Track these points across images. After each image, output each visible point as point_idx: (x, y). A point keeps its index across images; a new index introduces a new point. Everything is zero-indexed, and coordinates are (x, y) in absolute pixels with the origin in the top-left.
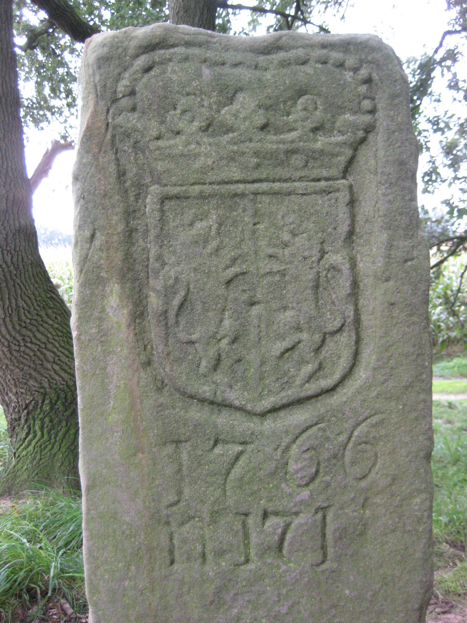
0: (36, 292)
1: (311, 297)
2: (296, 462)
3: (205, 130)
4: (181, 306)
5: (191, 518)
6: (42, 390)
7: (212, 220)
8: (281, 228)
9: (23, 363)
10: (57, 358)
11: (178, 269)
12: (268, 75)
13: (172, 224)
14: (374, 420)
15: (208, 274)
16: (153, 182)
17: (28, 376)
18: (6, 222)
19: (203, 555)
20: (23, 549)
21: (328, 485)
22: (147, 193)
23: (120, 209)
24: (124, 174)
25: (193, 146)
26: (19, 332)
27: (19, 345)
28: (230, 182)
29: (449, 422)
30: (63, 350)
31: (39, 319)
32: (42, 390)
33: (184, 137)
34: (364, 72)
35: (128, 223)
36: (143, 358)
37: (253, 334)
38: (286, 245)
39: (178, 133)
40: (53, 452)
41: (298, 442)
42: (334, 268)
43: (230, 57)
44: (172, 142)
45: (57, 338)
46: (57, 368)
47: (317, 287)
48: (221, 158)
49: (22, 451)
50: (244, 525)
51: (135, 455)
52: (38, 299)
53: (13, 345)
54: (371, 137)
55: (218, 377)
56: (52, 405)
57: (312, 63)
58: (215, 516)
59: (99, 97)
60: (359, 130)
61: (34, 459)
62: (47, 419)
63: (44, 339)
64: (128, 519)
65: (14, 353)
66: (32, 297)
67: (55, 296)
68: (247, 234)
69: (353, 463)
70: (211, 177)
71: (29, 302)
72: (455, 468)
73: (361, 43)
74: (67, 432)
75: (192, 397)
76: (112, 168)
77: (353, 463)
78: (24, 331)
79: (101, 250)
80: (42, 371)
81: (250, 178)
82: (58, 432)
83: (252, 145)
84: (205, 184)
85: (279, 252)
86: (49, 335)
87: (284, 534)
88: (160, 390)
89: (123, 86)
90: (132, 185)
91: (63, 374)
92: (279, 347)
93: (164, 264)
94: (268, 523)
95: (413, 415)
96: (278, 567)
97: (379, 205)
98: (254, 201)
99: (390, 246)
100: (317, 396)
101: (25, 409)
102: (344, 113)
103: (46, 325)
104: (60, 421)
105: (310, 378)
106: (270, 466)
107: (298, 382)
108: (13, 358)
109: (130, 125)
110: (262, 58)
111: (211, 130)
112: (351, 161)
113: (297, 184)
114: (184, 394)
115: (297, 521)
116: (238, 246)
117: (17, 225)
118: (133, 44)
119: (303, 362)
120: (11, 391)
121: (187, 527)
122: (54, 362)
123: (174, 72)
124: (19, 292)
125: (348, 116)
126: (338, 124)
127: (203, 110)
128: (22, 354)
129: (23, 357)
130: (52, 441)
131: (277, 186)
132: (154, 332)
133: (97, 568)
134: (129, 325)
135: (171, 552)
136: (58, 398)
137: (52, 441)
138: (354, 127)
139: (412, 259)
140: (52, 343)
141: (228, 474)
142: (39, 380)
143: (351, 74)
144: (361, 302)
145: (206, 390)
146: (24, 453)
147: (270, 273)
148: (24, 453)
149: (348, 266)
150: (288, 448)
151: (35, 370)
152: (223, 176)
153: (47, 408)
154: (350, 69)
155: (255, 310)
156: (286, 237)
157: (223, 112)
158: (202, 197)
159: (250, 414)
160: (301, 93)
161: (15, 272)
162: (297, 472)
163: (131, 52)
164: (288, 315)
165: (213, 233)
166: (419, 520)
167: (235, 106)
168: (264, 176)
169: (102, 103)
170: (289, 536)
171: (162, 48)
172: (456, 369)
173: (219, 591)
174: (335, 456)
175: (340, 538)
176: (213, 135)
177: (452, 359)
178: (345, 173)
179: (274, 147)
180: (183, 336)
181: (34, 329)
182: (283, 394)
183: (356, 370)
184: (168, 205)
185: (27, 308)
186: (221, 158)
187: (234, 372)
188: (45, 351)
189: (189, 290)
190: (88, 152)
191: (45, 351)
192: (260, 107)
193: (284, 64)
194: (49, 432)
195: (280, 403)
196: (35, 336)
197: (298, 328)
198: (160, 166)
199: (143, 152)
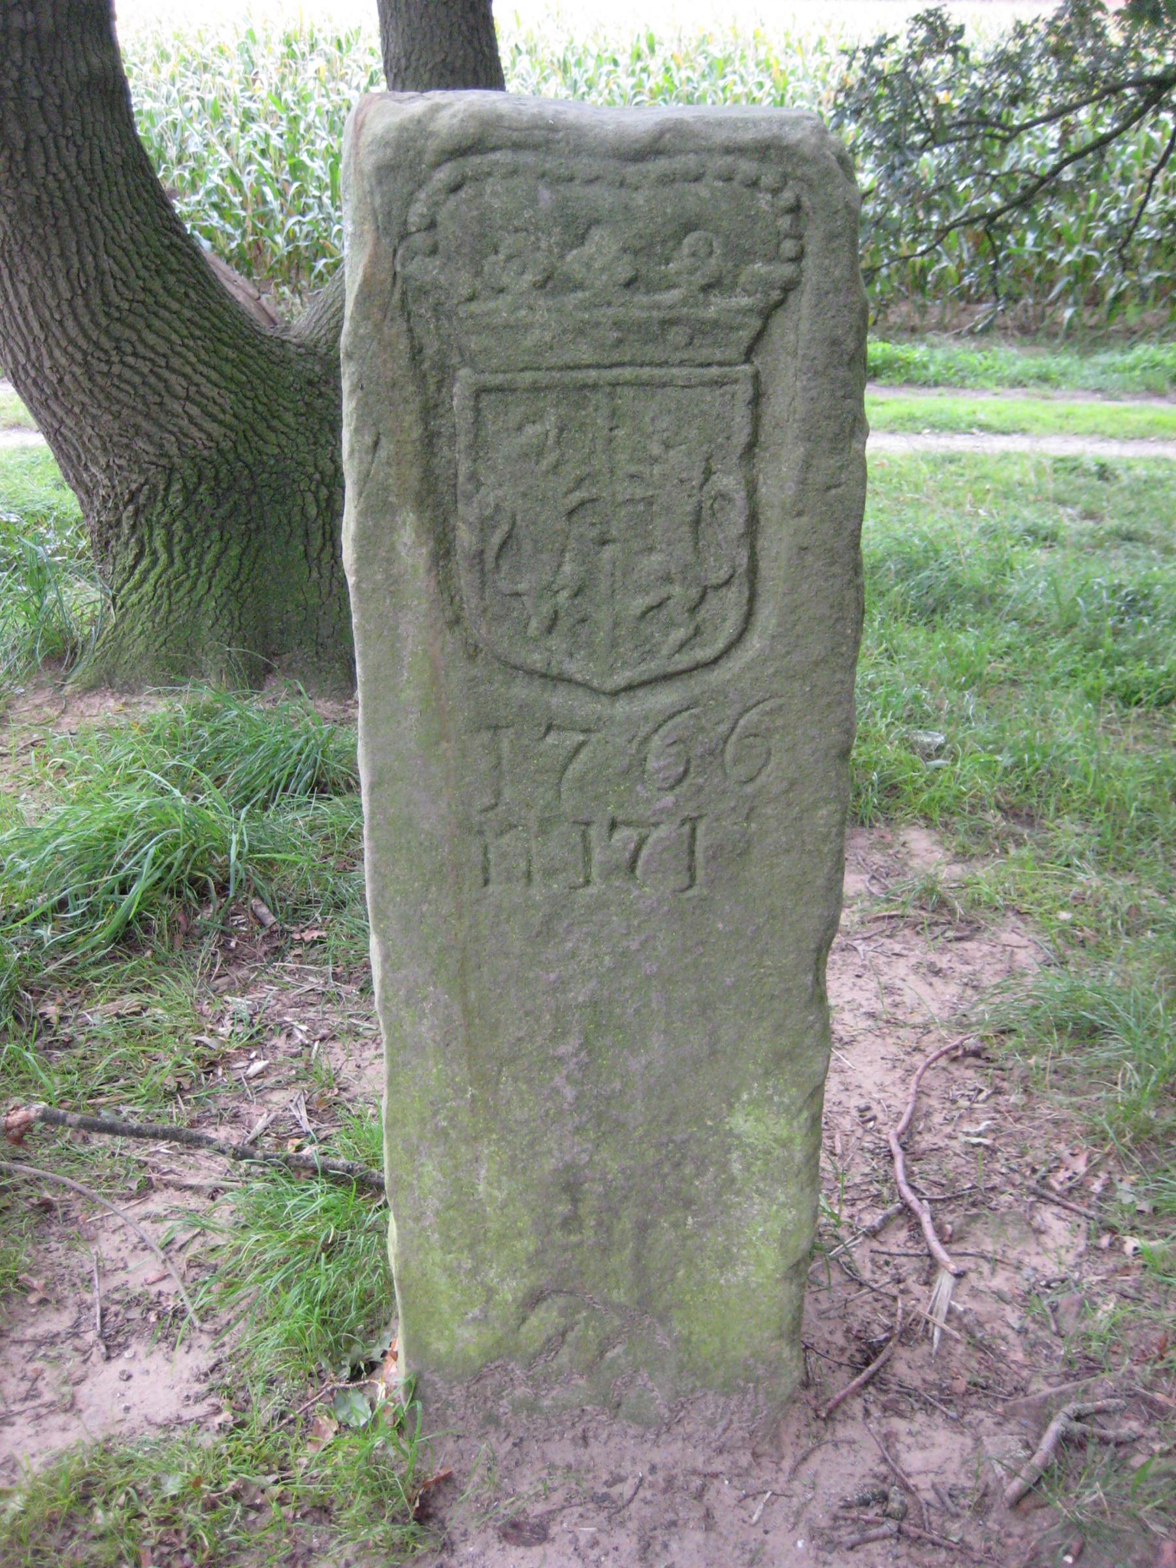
0: (139, 237)
1: (688, 537)
2: (658, 758)
3: (541, 286)
4: (504, 544)
5: (513, 826)
6: (164, 461)
7: (551, 419)
8: (649, 437)
9: (118, 402)
10: (193, 389)
11: (500, 493)
12: (640, 199)
13: (491, 428)
14: (767, 706)
15: (543, 500)
16: (463, 362)
17: (132, 431)
18: (57, 66)
19: (528, 875)
20: (175, 808)
21: (700, 789)
22: (454, 379)
23: (416, 405)
24: (420, 351)
25: (523, 313)
26: (107, 332)
28: (578, 367)
29: (1089, 515)
30: (205, 370)
31: (150, 300)
32: (164, 461)
33: (509, 298)
34: (788, 196)
35: (427, 424)
36: (449, 614)
37: (604, 586)
38: (655, 460)
39: (501, 291)
40: (196, 596)
41: (661, 732)
42: (722, 496)
43: (583, 166)
44: (492, 305)
46: (194, 411)
47: (697, 522)
48: (564, 332)
50: (584, 836)
51: (437, 743)
52: (145, 250)
53: (94, 362)
54: (791, 296)
55: (554, 642)
56: (189, 494)
57: (708, 179)
58: (545, 825)
59: (381, 231)
61: (157, 611)
62: (178, 526)
63: (163, 347)
64: (426, 826)
65: (98, 378)
66: (131, 247)
67: (179, 242)
68: (600, 445)
69: (736, 761)
70: (551, 359)
71: (125, 261)
72: (1064, 643)
73: (787, 147)
74: (223, 552)
75: (515, 667)
76: (403, 345)
77: (736, 761)
78: (117, 329)
79: (388, 464)
80: (163, 418)
81: (607, 362)
82: (203, 553)
83: (610, 311)
84: (539, 369)
85: (644, 469)
86: (174, 337)
87: (638, 850)
88: (472, 658)
89: (418, 211)
90: (432, 368)
92: (640, 603)
93: (479, 485)
94: (617, 836)
95: (825, 700)
96: (628, 891)
97: (796, 403)
98: (612, 396)
99: (807, 465)
100: (689, 671)
101: (131, 501)
102: (753, 262)
103: (163, 313)
104: (207, 530)
105: (682, 646)
106: (621, 763)
107: (665, 651)
108: (96, 390)
109: (428, 278)
110: (631, 169)
111: (550, 285)
112: (759, 336)
113: (675, 371)
114: (506, 664)
115: (656, 834)
116: (584, 462)
117: (84, 71)
118: (433, 145)
119: (672, 624)
120: (96, 462)
121: (506, 839)
122: (188, 398)
123: (494, 194)
124: (100, 236)
125: (759, 267)
126: (742, 279)
127: (539, 255)
130: (193, 572)
131: (646, 372)
132: (465, 580)
133: (385, 887)
134: (429, 570)
135: (485, 870)
136: (200, 478)
137: (193, 572)
138: (768, 285)
140: (179, 354)
141: (565, 768)
142: (156, 439)
143: (769, 197)
144: (761, 543)
145: (536, 659)
146: (134, 598)
148: (134, 598)
149: (743, 494)
150: (646, 739)
151: (147, 416)
152: (567, 358)
153: (176, 500)
154: (767, 190)
155: (608, 552)
156: (656, 449)
157: (569, 258)
159: (595, 691)
160: (689, 227)
161: (87, 190)
162: (658, 771)
163: (429, 157)
164: (656, 559)
165: (550, 442)
166: (825, 838)
167: (589, 249)
168: (627, 358)
169: (385, 241)
170: (644, 853)
172: (1137, 372)
173: (548, 920)
174: (711, 753)
175: (714, 857)
176: (553, 294)
177: (1131, 348)
178: (749, 355)
179: (645, 315)
180: (504, 586)
181: (140, 324)
182: (643, 667)
183: (748, 636)
184: (485, 400)
185: (120, 274)
186: (564, 332)
187: (575, 635)
188: (166, 374)
189: (514, 523)
190: (366, 318)
191: (166, 374)
192: (624, 250)
193: (666, 180)
194: (185, 552)
195: (638, 680)
196: (143, 341)
197: (668, 579)
198: (474, 343)
199: (449, 318)
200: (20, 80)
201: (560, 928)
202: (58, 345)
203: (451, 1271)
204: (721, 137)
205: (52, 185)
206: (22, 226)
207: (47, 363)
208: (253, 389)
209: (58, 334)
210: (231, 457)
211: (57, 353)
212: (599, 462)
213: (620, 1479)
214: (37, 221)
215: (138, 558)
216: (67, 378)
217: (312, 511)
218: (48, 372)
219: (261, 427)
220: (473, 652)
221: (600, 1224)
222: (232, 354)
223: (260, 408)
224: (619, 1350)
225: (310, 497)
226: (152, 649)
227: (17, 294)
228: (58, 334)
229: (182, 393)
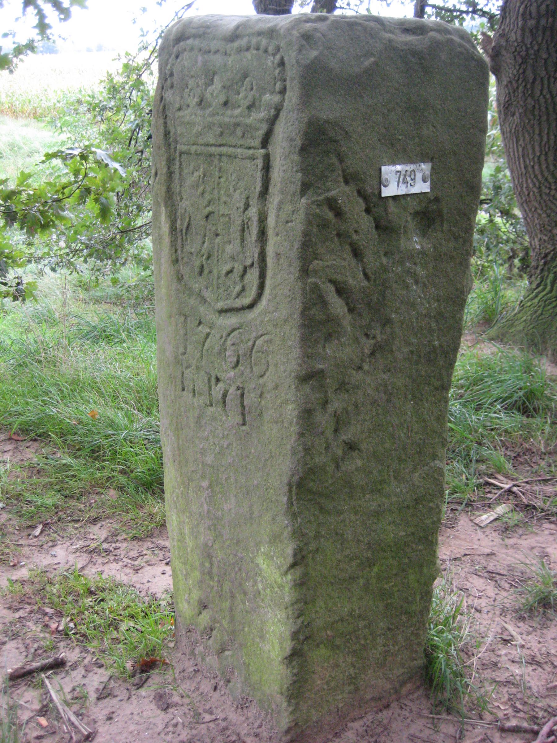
4: (188, 227)
9: (551, 209)
12: (230, 61)
13: (186, 171)
14: (266, 337)
23: (165, 158)
27: (550, 188)
34: (278, 57)
43: (214, 45)
47: (243, 230)
49: (528, 301)
53: (543, 188)
60: (271, 108)
70: (200, 141)
81: (217, 143)
98: (220, 161)
105: (238, 295)
106: (217, 348)
110: (229, 45)
113: (239, 150)
119: (235, 283)
128: (551, 199)
129: (552, 202)
139: (292, 221)
146: (529, 304)
158: (198, 155)
171: (183, 40)
184: (184, 157)
186: (205, 127)
193: (240, 50)
200: (538, 50)
202: (530, 177)
205: (542, 100)
206: (524, 119)
207: (525, 186)
209: (531, 172)
211: (529, 181)
213: (211, 713)
214: (531, 117)
215: (538, 286)
216: (531, 193)
218: (524, 189)
226: (526, 329)
227: (518, 151)
228: (531, 172)
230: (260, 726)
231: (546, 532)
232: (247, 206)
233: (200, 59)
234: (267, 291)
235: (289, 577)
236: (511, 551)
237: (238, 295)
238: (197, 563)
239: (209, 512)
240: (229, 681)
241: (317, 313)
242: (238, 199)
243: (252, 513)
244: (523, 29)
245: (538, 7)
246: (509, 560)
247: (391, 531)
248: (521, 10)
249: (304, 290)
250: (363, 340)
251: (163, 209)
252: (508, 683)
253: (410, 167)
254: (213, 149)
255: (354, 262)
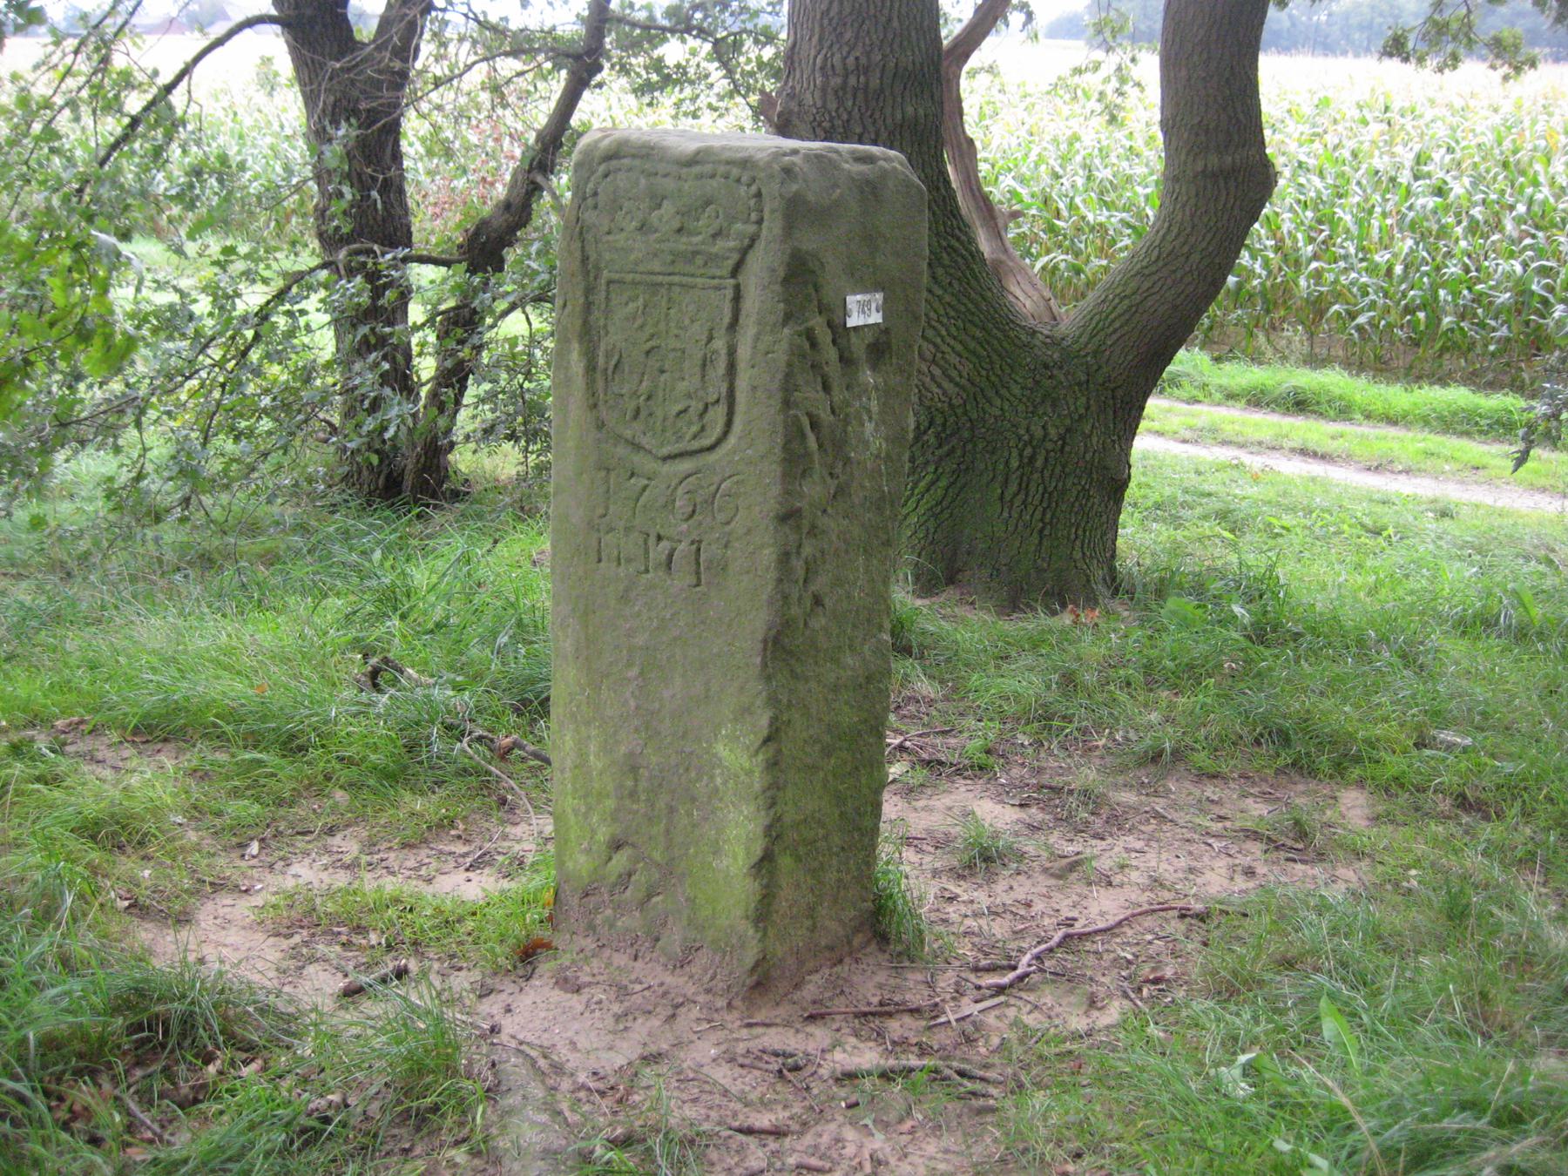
4: (616, 366)
7: (641, 301)
12: (686, 186)
14: (735, 479)
21: (700, 524)
23: (582, 286)
28: (652, 273)
34: (754, 188)
43: (662, 168)
45: (945, 321)
46: (937, 372)
47: (704, 365)
67: (957, 245)
70: (641, 268)
74: (933, 483)
76: (578, 254)
91: (946, 384)
98: (669, 289)
104: (927, 463)
105: (695, 437)
106: (662, 501)
107: (688, 437)
110: (685, 170)
113: (699, 280)
117: (899, 116)
118: (597, 154)
119: (690, 423)
131: (685, 280)
132: (600, 384)
135: (599, 552)
136: (931, 423)
140: (934, 328)
145: (628, 433)
147: (674, 350)
158: (635, 283)
160: (708, 203)
167: (662, 211)
173: (627, 590)
180: (616, 389)
184: (612, 287)
193: (700, 177)
201: (633, 594)
203: (576, 812)
204: (726, 155)
208: (991, 363)
210: (959, 411)
212: (662, 326)
217: (1015, 464)
219: (991, 393)
220: (600, 425)
221: (648, 800)
222: (978, 334)
223: (993, 378)
224: (659, 898)
225: (1015, 453)
229: (928, 355)
230: (712, 979)
231: (963, 789)
232: (710, 339)
233: (643, 181)
234: (738, 426)
235: (761, 757)
236: (923, 814)
237: (695, 437)
238: (610, 787)
239: (637, 708)
240: (657, 940)
241: (795, 445)
242: (698, 330)
243: (708, 690)
244: (824, 90)
245: (844, 59)
246: (923, 824)
247: (848, 717)
248: (818, 61)
249: (785, 421)
250: (828, 479)
251: (576, 346)
252: (966, 934)
253: (867, 297)
254: (660, 278)
255: (822, 394)
